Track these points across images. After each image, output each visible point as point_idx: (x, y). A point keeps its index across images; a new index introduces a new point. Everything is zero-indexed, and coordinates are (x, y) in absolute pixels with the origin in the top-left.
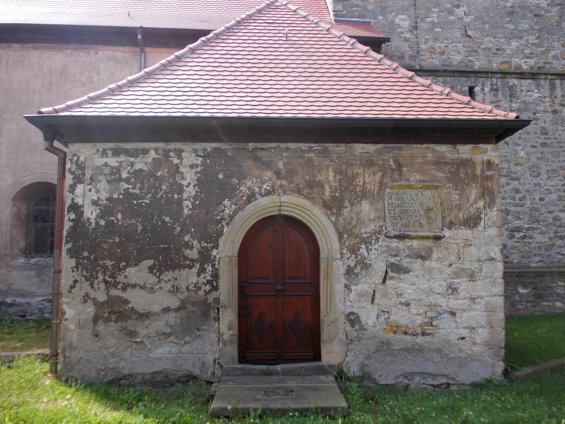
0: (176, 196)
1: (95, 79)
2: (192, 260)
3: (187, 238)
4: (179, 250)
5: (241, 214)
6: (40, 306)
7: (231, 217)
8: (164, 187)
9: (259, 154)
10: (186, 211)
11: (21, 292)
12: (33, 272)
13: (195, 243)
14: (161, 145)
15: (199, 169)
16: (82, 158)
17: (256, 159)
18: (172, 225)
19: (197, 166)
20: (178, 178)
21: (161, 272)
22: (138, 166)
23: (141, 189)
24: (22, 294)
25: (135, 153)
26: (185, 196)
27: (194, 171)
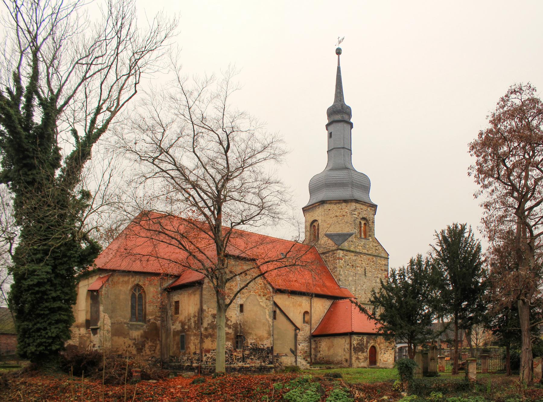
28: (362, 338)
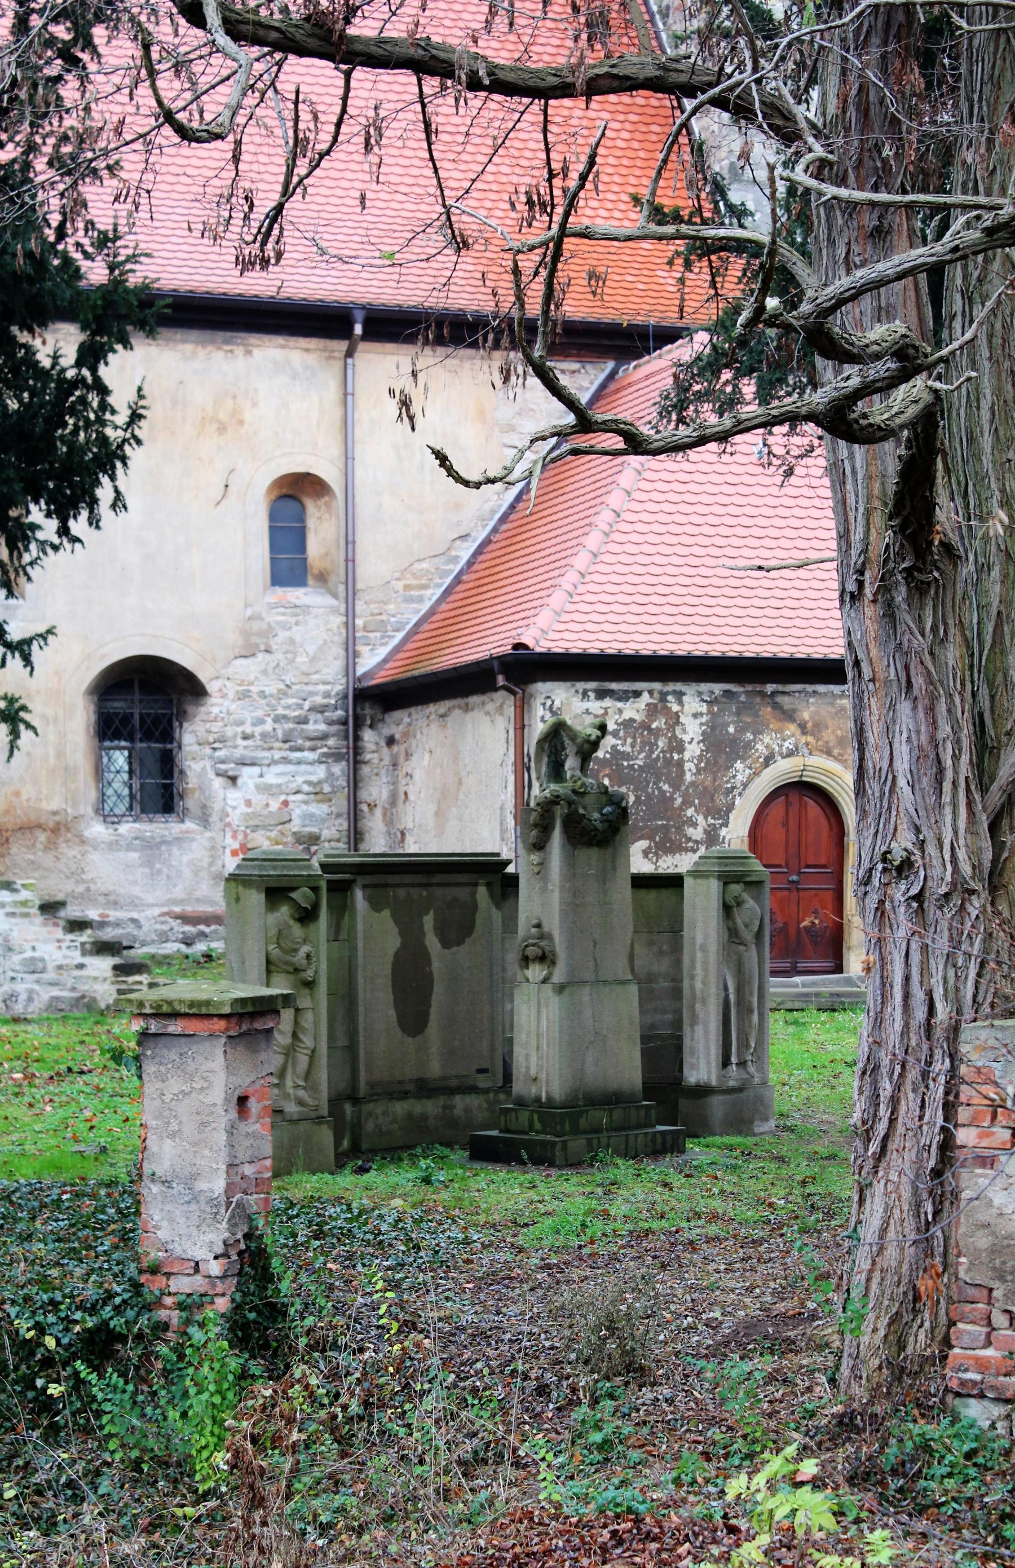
0: (676, 756)
1: (247, 416)
2: (697, 842)
3: (690, 812)
4: (680, 830)
5: (758, 780)
6: (158, 926)
7: (745, 785)
8: (661, 744)
9: (779, 699)
10: (688, 777)
11: (112, 898)
12: (135, 855)
13: (700, 819)
14: (657, 686)
15: (704, 719)
16: (557, 704)
17: (777, 707)
18: (672, 794)
19: (701, 714)
20: (678, 731)
21: (658, 857)
22: (627, 715)
23: (633, 746)
24: (116, 903)
25: (623, 697)
26: (687, 755)
27: (698, 721)
28: (652, 711)
